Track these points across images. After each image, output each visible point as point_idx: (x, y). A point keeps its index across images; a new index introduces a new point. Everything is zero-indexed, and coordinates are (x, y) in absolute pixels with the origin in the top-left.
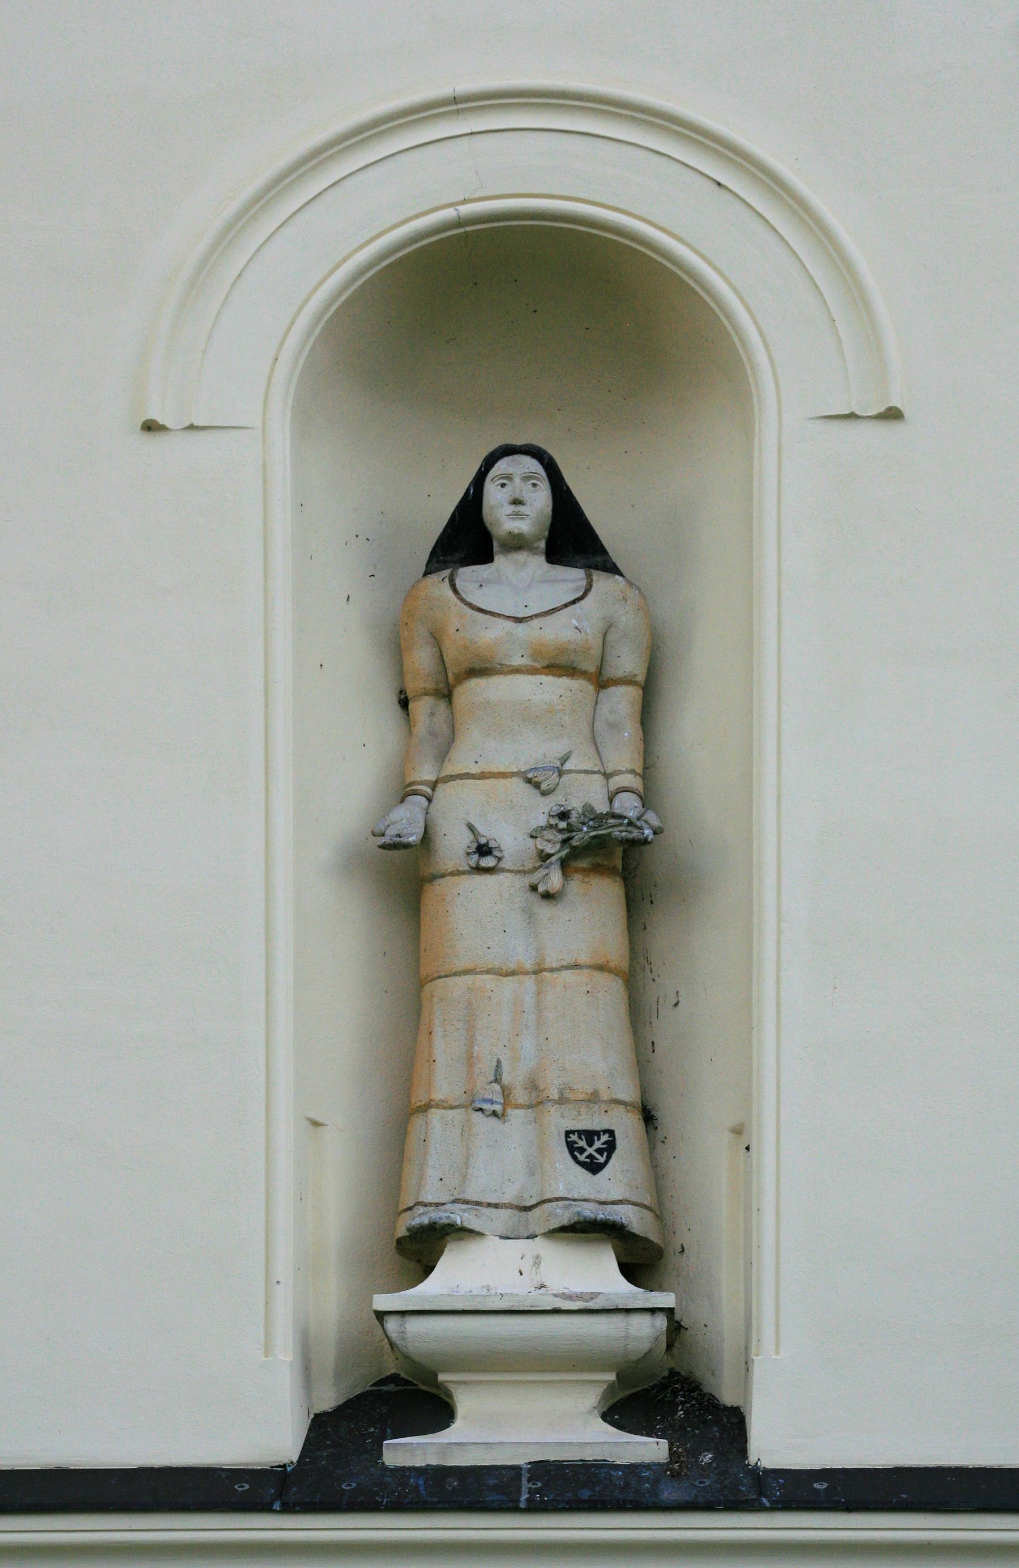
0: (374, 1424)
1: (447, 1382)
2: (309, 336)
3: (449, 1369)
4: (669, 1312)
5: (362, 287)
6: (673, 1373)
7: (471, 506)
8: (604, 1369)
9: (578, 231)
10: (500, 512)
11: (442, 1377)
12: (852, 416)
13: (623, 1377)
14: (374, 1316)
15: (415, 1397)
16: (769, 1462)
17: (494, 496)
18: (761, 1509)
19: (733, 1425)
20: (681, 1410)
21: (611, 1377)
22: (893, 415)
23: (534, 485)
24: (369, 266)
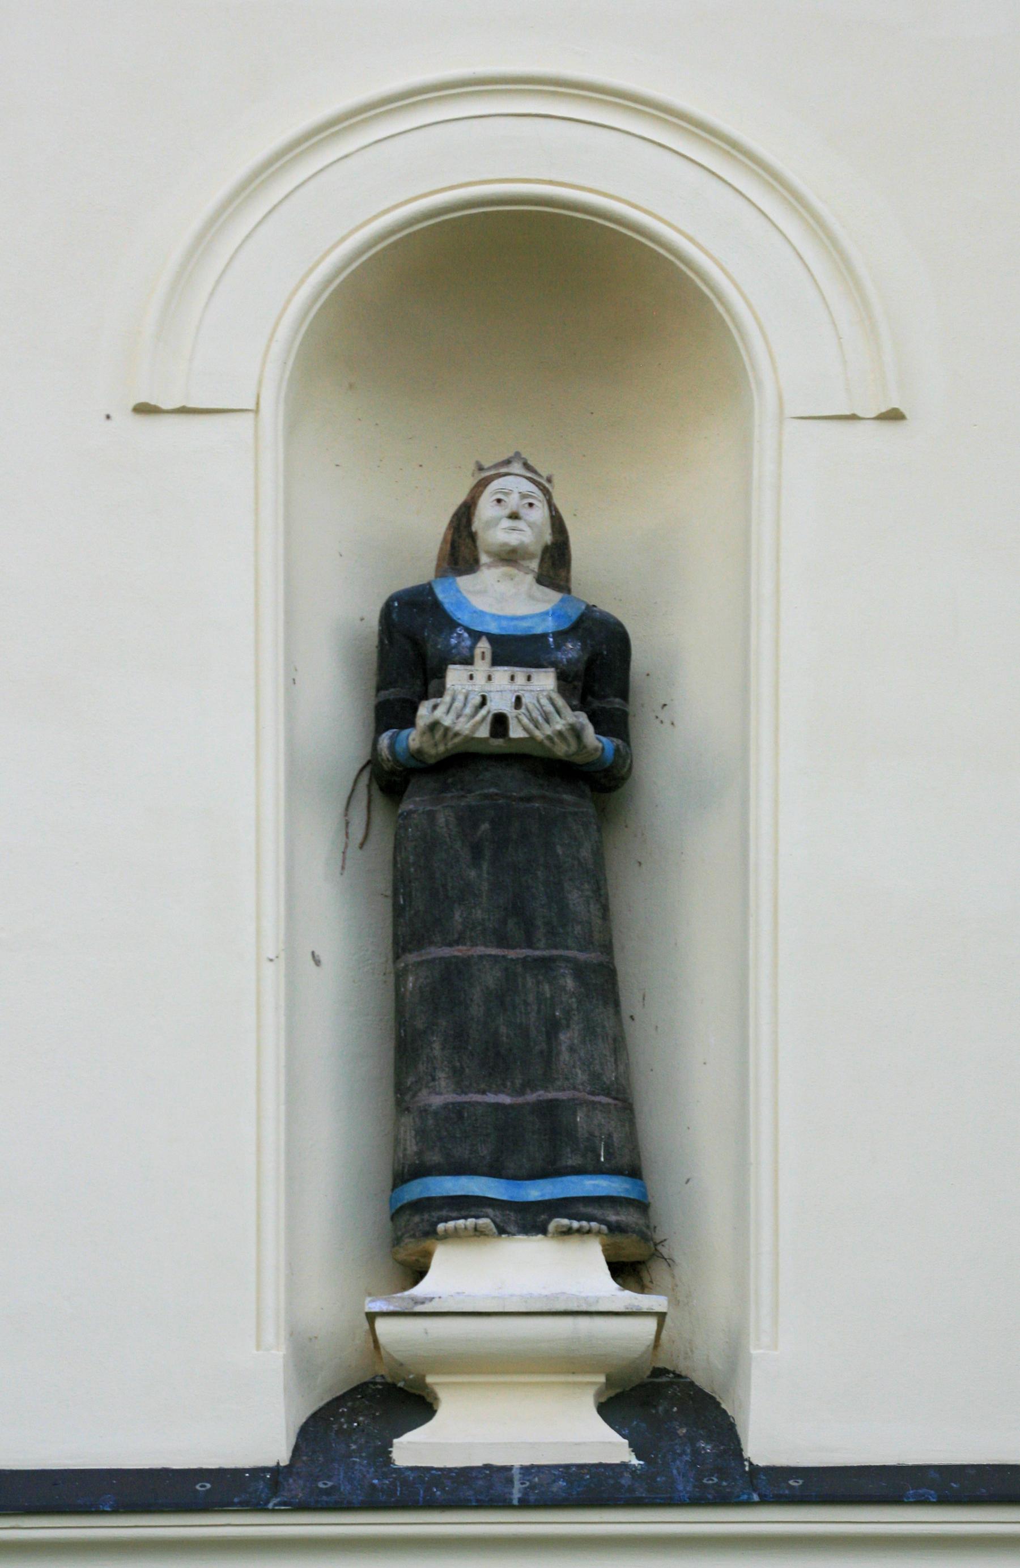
0: (358, 1427)
1: (437, 1384)
2: (296, 332)
3: (437, 1373)
4: (661, 1316)
5: (324, 306)
6: (658, 1372)
7: (463, 521)
8: (593, 1370)
9: (678, 268)
10: (494, 528)
11: (430, 1379)
12: (853, 417)
13: (610, 1382)
14: (364, 1316)
15: (399, 1398)
16: (761, 1461)
17: (486, 510)
18: (748, 1503)
19: (725, 1432)
20: (675, 1427)
21: (602, 1379)
22: (894, 416)
23: (531, 505)
24: (329, 282)
